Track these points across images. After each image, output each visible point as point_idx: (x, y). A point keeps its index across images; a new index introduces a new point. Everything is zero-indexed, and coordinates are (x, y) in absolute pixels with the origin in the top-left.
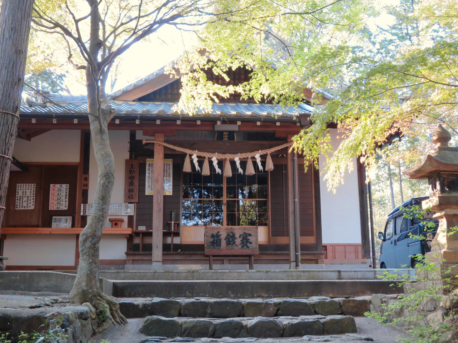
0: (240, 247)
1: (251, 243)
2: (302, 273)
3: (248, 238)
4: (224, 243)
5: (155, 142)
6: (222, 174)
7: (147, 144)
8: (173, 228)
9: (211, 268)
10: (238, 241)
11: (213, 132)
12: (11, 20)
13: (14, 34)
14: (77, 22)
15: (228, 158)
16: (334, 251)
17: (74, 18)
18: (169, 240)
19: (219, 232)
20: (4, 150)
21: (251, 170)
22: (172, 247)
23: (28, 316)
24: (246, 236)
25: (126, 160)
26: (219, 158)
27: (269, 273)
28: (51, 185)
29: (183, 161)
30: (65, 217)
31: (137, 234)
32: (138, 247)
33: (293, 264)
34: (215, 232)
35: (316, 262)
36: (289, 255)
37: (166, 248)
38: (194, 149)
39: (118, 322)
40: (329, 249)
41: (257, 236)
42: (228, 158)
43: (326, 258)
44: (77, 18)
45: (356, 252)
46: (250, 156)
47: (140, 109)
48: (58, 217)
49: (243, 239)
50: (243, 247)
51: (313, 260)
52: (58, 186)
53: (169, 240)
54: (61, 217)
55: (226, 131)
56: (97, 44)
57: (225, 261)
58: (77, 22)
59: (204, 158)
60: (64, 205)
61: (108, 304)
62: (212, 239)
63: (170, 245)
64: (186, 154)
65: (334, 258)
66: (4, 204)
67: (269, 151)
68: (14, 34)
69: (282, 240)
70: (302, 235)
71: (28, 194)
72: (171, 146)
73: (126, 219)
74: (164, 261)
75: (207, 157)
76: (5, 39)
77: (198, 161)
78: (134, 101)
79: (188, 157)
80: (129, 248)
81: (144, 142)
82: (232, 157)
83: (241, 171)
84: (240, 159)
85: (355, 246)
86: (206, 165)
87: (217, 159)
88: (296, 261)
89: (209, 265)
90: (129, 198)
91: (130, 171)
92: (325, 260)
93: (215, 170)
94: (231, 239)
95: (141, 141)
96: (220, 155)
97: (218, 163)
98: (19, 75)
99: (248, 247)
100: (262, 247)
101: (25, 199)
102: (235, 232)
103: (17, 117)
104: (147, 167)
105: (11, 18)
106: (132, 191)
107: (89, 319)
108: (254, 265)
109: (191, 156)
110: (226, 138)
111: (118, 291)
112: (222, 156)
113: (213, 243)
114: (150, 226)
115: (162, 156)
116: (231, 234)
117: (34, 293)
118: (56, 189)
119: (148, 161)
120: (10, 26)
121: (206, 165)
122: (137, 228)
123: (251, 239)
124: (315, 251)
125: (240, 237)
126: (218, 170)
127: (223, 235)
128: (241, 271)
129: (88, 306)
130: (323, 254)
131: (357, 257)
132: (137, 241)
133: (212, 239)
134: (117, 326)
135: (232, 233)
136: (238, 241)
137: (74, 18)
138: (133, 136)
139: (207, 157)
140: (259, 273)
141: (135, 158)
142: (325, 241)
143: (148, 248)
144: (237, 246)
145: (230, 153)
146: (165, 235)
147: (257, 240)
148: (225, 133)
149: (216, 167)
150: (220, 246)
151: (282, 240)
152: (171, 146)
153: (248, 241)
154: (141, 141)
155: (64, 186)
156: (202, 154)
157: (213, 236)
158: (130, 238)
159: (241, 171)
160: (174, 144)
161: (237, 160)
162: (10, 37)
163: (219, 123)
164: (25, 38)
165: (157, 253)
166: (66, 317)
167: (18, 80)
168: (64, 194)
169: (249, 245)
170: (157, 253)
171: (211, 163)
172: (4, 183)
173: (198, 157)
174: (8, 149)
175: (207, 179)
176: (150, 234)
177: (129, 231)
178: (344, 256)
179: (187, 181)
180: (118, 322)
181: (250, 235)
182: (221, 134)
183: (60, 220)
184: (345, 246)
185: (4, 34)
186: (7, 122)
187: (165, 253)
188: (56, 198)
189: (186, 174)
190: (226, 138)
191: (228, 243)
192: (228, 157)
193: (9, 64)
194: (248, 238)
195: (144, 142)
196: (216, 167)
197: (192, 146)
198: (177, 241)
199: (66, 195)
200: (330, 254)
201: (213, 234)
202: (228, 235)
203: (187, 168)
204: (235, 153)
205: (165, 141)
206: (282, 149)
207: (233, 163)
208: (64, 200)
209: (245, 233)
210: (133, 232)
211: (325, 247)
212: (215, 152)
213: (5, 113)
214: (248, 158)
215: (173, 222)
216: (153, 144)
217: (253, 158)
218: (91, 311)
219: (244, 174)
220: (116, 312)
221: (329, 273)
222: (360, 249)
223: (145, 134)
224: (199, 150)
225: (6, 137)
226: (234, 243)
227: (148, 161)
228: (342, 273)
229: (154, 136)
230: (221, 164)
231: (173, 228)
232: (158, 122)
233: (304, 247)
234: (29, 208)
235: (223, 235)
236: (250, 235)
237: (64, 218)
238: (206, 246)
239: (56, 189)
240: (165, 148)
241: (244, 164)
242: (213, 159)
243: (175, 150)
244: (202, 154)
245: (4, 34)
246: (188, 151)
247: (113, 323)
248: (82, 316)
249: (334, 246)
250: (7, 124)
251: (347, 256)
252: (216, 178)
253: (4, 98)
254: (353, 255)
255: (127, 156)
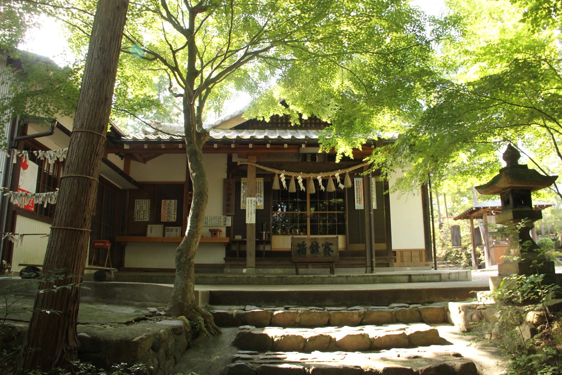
0: (323, 254)
1: (332, 251)
2: (378, 278)
3: (330, 246)
4: (308, 252)
5: (248, 163)
6: (288, 190)
7: (241, 165)
8: (264, 237)
9: (297, 273)
10: (321, 249)
11: (299, 154)
12: (100, 41)
13: (102, 54)
14: (174, 52)
15: (312, 177)
16: (402, 256)
17: (171, 48)
18: (261, 248)
19: (304, 242)
20: (88, 171)
21: (332, 188)
22: (264, 254)
23: (117, 340)
24: (328, 245)
25: (224, 180)
26: (304, 177)
27: (349, 278)
28: (163, 201)
29: (273, 180)
30: (176, 228)
31: (235, 242)
32: (235, 253)
33: (369, 269)
34: (301, 242)
35: (388, 265)
36: (366, 259)
37: (259, 254)
38: (282, 170)
39: (212, 334)
40: (398, 254)
41: (337, 245)
42: (312, 177)
43: (395, 261)
44: (174, 48)
45: (421, 256)
46: (331, 175)
47: (233, 135)
48: (170, 228)
49: (326, 248)
50: (325, 254)
51: (384, 264)
52: (168, 201)
53: (261, 248)
54: (173, 228)
55: (309, 154)
56: (193, 73)
57: (309, 266)
58: (174, 52)
59: (291, 176)
60: (173, 217)
61: (202, 316)
62: (298, 248)
63: (262, 251)
64: (275, 174)
65: (402, 261)
66: (90, 226)
67: (348, 171)
68: (102, 54)
69: (359, 247)
70: (376, 242)
71: (144, 208)
72: (262, 167)
73: (224, 230)
74: (257, 266)
75: (293, 176)
76: (93, 60)
77: (285, 180)
78: (231, 129)
79: (277, 176)
80: (227, 254)
81: (239, 164)
82: (315, 176)
83: (322, 188)
84: (322, 177)
85: (420, 251)
86: (293, 183)
87: (302, 178)
88: (372, 266)
89: (295, 269)
90: (226, 211)
91: (228, 189)
92: (394, 264)
93: (300, 187)
94: (315, 248)
95: (236, 163)
96: (305, 174)
97: (302, 182)
98: (106, 95)
99: (330, 255)
100: (342, 254)
101: (142, 212)
102: (318, 242)
103: (103, 137)
104: (242, 185)
105: (100, 39)
106: (230, 205)
107: (184, 333)
108: (336, 269)
109: (279, 175)
110: (309, 160)
111: (215, 299)
112: (307, 176)
113: (299, 251)
114: (244, 236)
115: (254, 175)
116: (315, 244)
117: (137, 303)
118: (167, 204)
119: (243, 180)
120: (99, 46)
121: (293, 183)
122: (234, 237)
123: (333, 248)
124: (388, 256)
125: (322, 246)
126: (302, 188)
127: (308, 244)
128: (324, 276)
129: (184, 320)
130: (392, 259)
131: (421, 260)
132: (234, 248)
133: (298, 248)
134: (211, 338)
135: (316, 242)
136: (321, 249)
137: (171, 48)
138: (230, 158)
139: (293, 176)
140: (339, 278)
141: (232, 178)
142: (394, 247)
143: (243, 255)
144: (320, 254)
145: (313, 173)
146: (258, 243)
147: (338, 248)
148: (308, 155)
149: (301, 185)
150: (305, 254)
151: (359, 247)
152: (262, 167)
153: (329, 249)
154: (236, 163)
155: (173, 201)
156: (289, 174)
157: (299, 245)
158: (228, 247)
159: (322, 188)
160: (264, 165)
161: (319, 178)
162: (99, 57)
163: (303, 146)
164: (114, 58)
165: (251, 259)
166: (157, 336)
167: (105, 100)
168: (173, 208)
169: (330, 253)
170: (251, 259)
171: (296, 181)
172: (88, 205)
173: (285, 176)
174: (93, 170)
175: (293, 195)
176: (245, 243)
177: (227, 240)
178: (410, 259)
179: (274, 196)
180: (212, 334)
181: (331, 244)
182: (305, 155)
183: (172, 230)
184: (411, 251)
185: (92, 55)
186: (92, 141)
187: (258, 258)
188: (166, 212)
189: (275, 191)
190: (309, 160)
191: (312, 252)
192: (312, 176)
193: (96, 83)
194: (330, 246)
195: (239, 164)
196: (301, 185)
197: (280, 167)
198: (268, 248)
199: (175, 209)
200: (398, 257)
201: (299, 244)
202: (312, 244)
203: (276, 186)
204: (318, 172)
205: (257, 163)
206: (358, 169)
207: (316, 181)
208: (173, 213)
209: (327, 243)
210: (230, 241)
211: (395, 252)
212: (299, 172)
213: (90, 132)
214: (329, 177)
215: (264, 232)
216: (247, 165)
217: (334, 176)
218: (186, 324)
219: (325, 190)
220: (210, 324)
221: (401, 277)
222: (424, 253)
223: (240, 156)
224: (286, 171)
225: (91, 157)
226: (318, 251)
227: (243, 180)
228: (412, 277)
229: (247, 158)
230: (305, 182)
231: (264, 237)
232: (251, 146)
233: (378, 253)
234: (145, 220)
235: (308, 244)
236: (331, 244)
237: (174, 228)
238: (293, 254)
239: (167, 204)
240: (257, 168)
241: (325, 182)
242: (298, 178)
243: (265, 171)
244: (289, 174)
245: (92, 55)
246: (277, 172)
247: (207, 335)
248: (175, 331)
249: (402, 251)
250: (92, 143)
251: (413, 260)
252: (302, 194)
253: (90, 117)
254: (418, 259)
255: (225, 176)
